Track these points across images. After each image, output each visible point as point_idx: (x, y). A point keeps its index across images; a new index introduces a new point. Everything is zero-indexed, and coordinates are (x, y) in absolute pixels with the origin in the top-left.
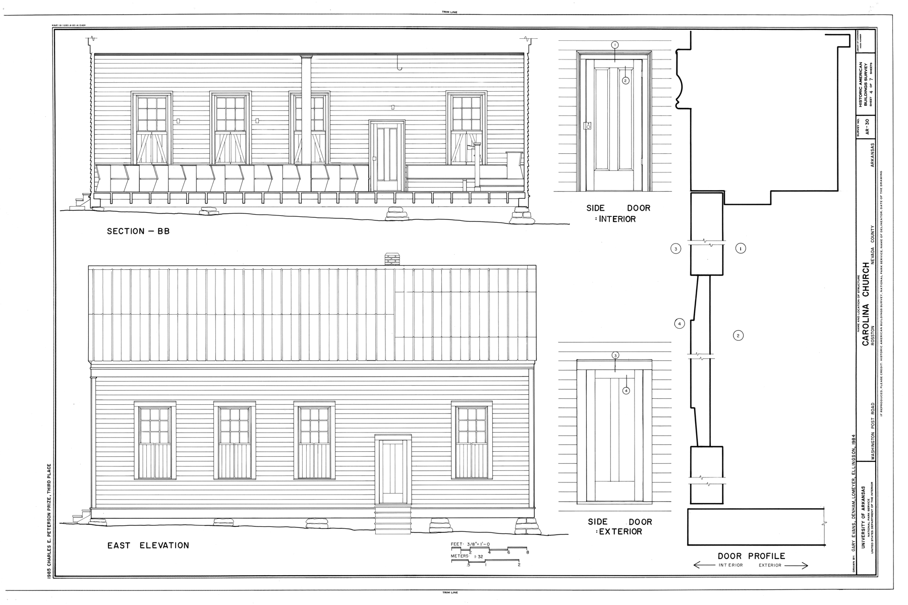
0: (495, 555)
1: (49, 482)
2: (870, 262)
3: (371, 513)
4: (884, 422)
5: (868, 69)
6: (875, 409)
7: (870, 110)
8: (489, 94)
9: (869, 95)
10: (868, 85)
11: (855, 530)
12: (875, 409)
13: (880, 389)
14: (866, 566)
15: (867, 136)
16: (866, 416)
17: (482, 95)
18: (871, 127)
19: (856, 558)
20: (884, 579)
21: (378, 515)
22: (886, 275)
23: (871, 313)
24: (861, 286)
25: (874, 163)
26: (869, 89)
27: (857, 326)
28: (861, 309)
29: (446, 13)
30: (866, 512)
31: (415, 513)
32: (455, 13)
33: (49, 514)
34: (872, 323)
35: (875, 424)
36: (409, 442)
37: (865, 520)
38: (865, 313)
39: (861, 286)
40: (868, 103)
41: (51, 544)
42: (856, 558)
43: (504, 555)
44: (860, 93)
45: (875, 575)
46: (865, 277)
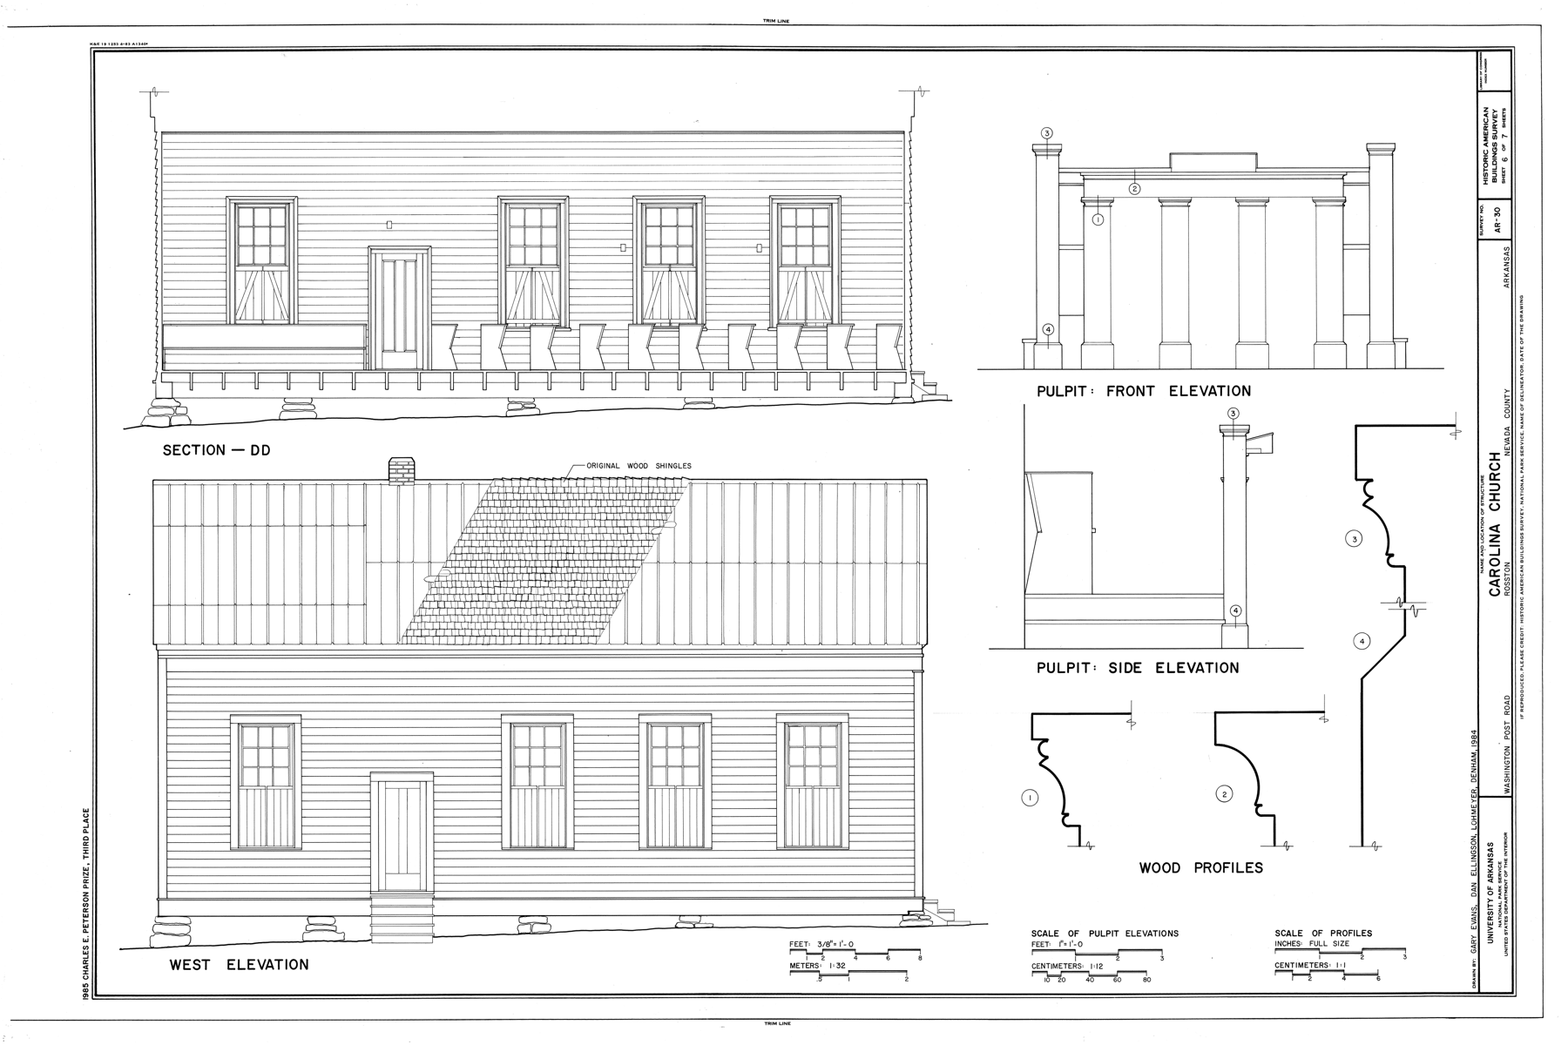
0: (864, 963)
1: (86, 839)
2: (1503, 452)
3: (364, 907)
4: (1527, 729)
5: (1499, 119)
6: (1511, 705)
7: (1503, 190)
8: (301, 202)
9: (1500, 164)
10: (1499, 147)
11: (1476, 918)
12: (1512, 705)
13: (1519, 673)
14: (1495, 978)
15: (1497, 235)
16: (1494, 721)
17: (288, 204)
18: (1505, 220)
19: (1477, 964)
20: (1526, 1001)
21: (376, 911)
22: (1531, 474)
23: (1505, 540)
24: (1487, 492)
25: (1510, 281)
26: (1500, 155)
27: (1480, 563)
28: (1487, 533)
29: (769, 22)
30: (1495, 885)
31: (440, 908)
32: (785, 23)
33: (86, 894)
34: (1505, 557)
35: (1511, 731)
36: (430, 785)
37: (1495, 896)
38: (1495, 539)
39: (1487, 492)
40: (1499, 178)
41: (89, 944)
42: (1477, 964)
43: (880, 963)
44: (1485, 160)
45: (1512, 993)
46: (1494, 477)
